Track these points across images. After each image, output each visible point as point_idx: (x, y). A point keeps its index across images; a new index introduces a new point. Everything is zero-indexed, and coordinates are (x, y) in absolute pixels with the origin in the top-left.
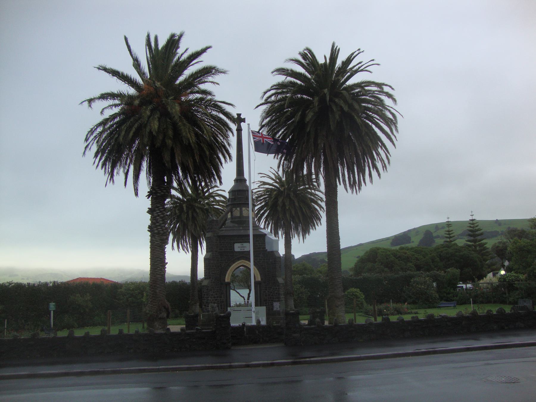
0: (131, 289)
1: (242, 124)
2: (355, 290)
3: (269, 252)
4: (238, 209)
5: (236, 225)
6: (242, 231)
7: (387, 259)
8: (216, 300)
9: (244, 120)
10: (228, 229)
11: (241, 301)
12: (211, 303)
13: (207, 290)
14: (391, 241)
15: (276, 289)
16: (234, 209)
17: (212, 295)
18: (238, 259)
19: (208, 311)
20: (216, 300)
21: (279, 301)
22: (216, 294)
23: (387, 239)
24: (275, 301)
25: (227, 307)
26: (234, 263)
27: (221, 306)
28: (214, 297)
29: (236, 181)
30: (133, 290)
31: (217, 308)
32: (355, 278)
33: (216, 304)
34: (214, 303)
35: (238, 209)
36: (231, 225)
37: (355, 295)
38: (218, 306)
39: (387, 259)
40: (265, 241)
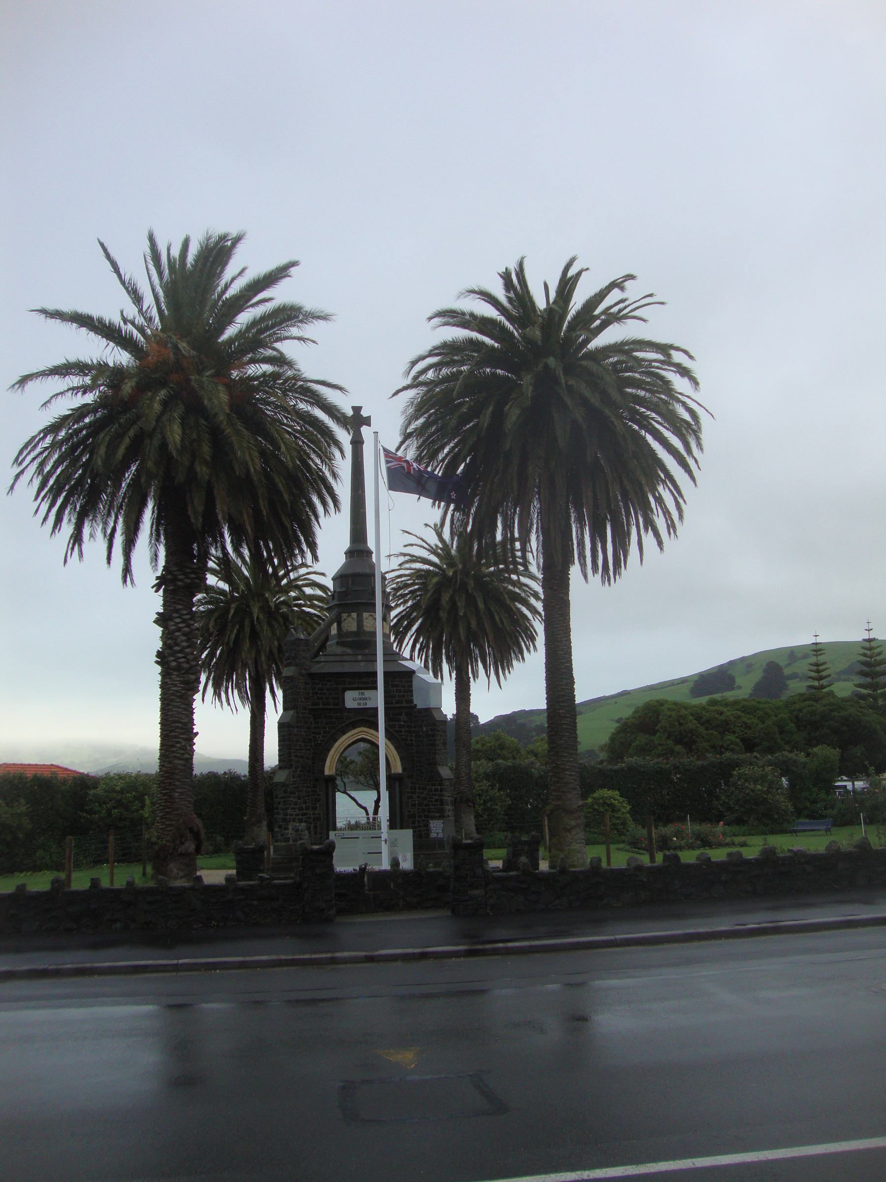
0: (118, 788)
1: (364, 429)
2: (610, 793)
3: (420, 710)
4: (354, 615)
5: (349, 651)
6: (362, 664)
7: (680, 724)
8: (306, 814)
9: (367, 421)
10: (331, 658)
11: (360, 816)
12: (294, 820)
13: (285, 792)
14: (691, 685)
15: (436, 790)
16: (344, 615)
17: (295, 804)
18: (354, 726)
19: (287, 840)
20: (306, 814)
21: (441, 817)
22: (305, 802)
23: (683, 681)
24: (433, 818)
25: (328, 831)
26: (344, 733)
27: (315, 827)
28: (301, 809)
29: (350, 553)
30: (122, 791)
31: (307, 832)
32: (610, 767)
33: (303, 824)
34: (301, 821)
35: (354, 615)
36: (339, 650)
37: (608, 805)
38: (308, 829)
39: (680, 724)
40: (411, 686)
